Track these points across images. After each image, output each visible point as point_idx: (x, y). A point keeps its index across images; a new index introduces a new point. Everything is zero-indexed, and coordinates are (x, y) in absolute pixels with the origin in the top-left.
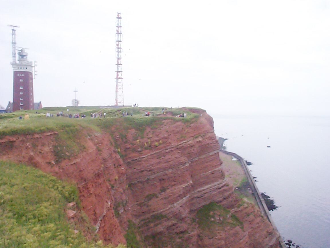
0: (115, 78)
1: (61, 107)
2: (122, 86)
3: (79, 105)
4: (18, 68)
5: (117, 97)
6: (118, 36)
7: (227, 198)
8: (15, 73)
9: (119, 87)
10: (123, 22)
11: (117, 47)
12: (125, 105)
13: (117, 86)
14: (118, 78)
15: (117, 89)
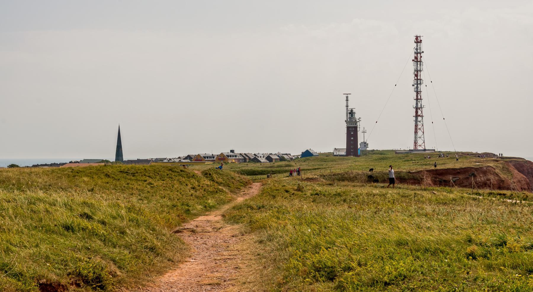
0: (352, 131)
1: (529, 161)
3: (368, 149)
6: (417, 65)
7: (173, 171)
9: (419, 127)
10: (424, 46)
12: (427, 148)
13: (416, 126)
14: (417, 116)
15: (416, 129)
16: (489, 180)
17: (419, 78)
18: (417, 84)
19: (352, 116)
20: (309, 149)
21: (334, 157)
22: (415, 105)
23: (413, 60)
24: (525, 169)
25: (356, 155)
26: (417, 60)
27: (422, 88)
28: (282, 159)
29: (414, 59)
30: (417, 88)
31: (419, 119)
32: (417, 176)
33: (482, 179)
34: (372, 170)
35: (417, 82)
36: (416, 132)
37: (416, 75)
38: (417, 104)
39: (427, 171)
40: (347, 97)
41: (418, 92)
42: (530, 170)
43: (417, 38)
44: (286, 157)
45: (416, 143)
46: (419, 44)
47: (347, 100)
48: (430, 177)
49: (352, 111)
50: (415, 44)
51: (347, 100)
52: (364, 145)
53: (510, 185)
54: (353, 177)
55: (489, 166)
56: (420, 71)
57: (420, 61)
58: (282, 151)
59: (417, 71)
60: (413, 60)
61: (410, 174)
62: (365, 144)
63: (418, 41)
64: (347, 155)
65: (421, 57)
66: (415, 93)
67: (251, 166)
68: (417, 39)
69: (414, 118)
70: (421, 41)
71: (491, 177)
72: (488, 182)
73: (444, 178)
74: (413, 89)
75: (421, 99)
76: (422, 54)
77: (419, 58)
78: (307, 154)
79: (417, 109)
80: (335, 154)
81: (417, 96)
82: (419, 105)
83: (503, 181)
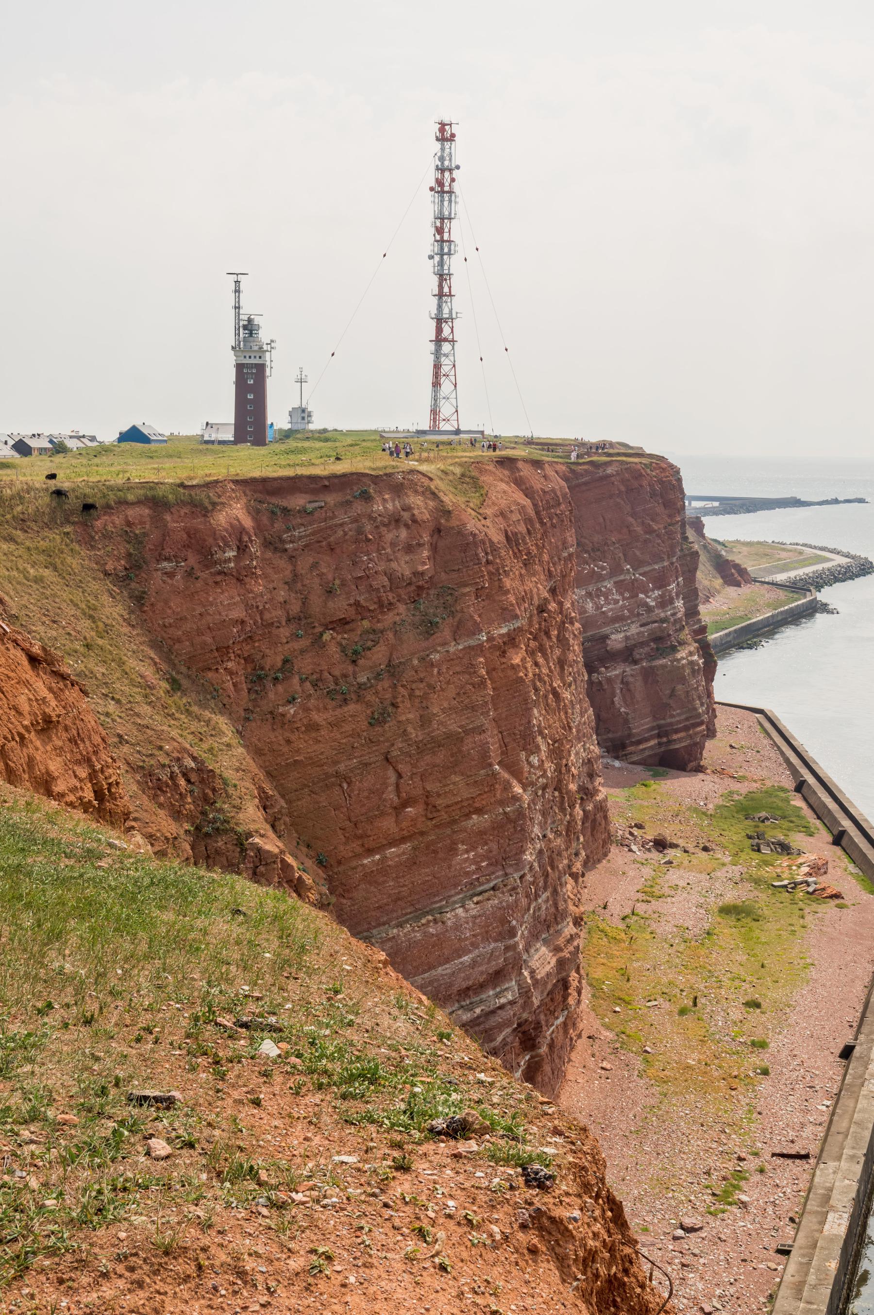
0: (251, 382)
2: (454, 366)
3: (311, 427)
4: (245, 357)
5: (436, 400)
6: (442, 201)
8: (239, 367)
9: (445, 369)
10: (460, 152)
11: (438, 237)
12: (462, 428)
13: (437, 367)
14: (439, 340)
16: (407, 508)
17: (446, 237)
18: (442, 255)
19: (251, 334)
20: (138, 424)
21: (205, 446)
22: (434, 311)
23: (432, 189)
24: (645, 483)
25: (260, 440)
26: (442, 189)
27: (454, 264)
28: (58, 448)
29: (433, 183)
30: (441, 263)
31: (446, 347)
32: (201, 496)
33: (390, 506)
34: (52, 476)
35: (442, 249)
36: (436, 384)
37: (440, 231)
38: (440, 307)
39: (236, 482)
40: (237, 282)
41: (443, 277)
42: (657, 487)
43: (443, 126)
44: (72, 444)
45: (435, 412)
46: (447, 145)
47: (237, 291)
48: (244, 500)
49: (250, 320)
50: (438, 145)
51: (237, 291)
52: (300, 414)
53: (464, 525)
54: (12, 498)
55: (412, 471)
56: (450, 219)
57: (451, 192)
58: (61, 429)
59: (442, 219)
60: (432, 189)
61: (182, 490)
62: (302, 413)
63: (445, 135)
64: (235, 442)
65: (453, 180)
66: (435, 279)
67: (160, 438)
68: (442, 130)
69: (432, 347)
70: (453, 135)
71: (416, 501)
72: (406, 515)
73: (284, 503)
74: (429, 267)
75: (450, 295)
76: (456, 174)
77: (447, 184)
78: (134, 435)
79: (440, 321)
80: (206, 438)
81: (441, 287)
82: (446, 310)
83: (448, 513)
